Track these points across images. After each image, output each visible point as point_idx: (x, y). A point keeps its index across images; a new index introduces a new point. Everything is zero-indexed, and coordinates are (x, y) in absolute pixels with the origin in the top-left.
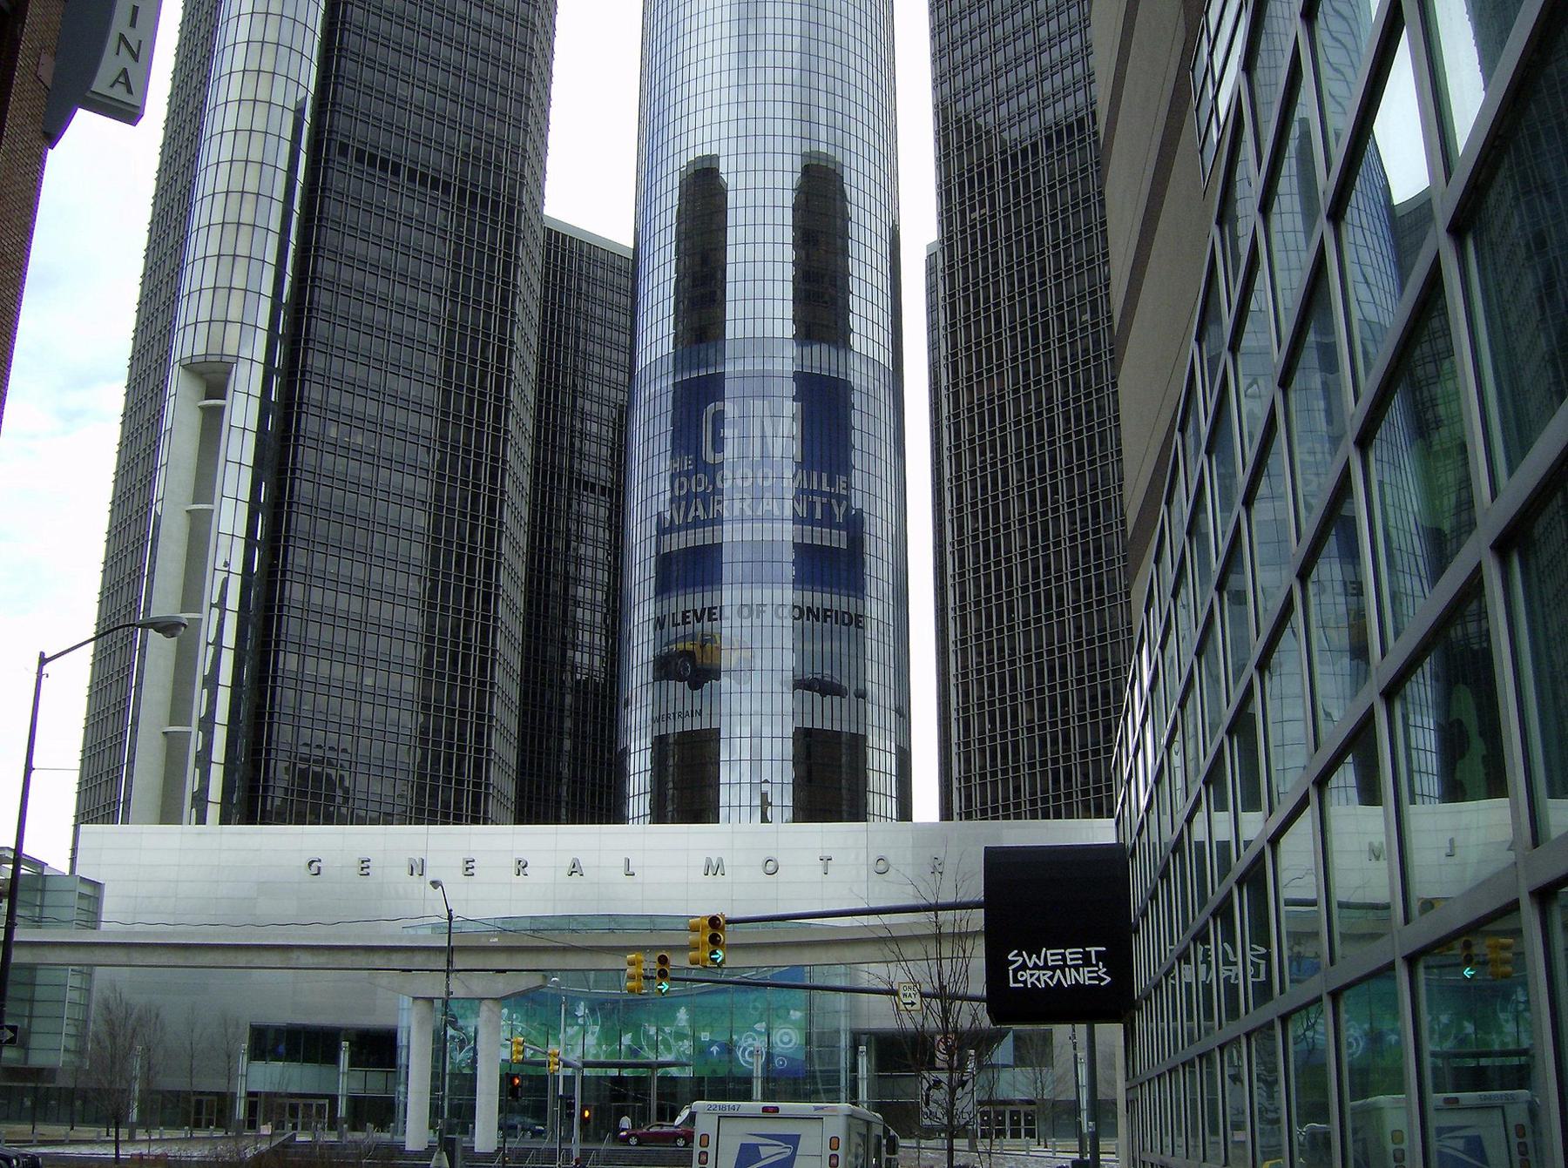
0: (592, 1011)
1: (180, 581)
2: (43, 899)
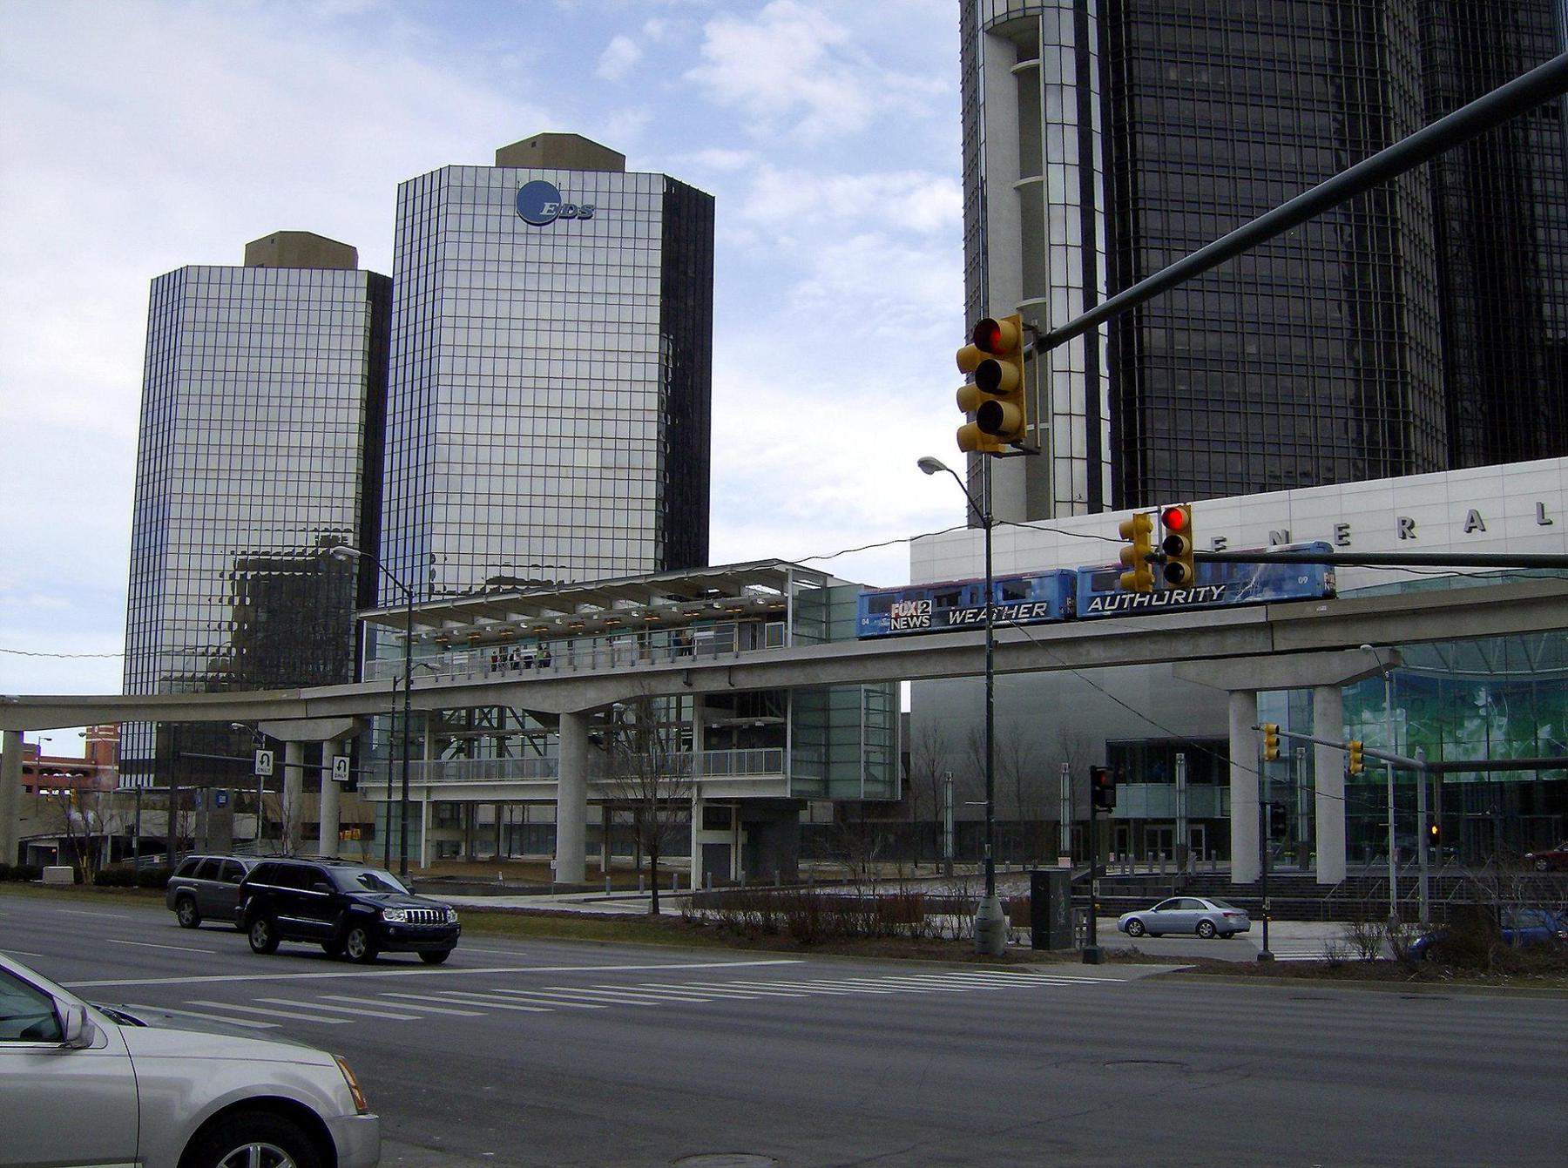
0: (1497, 698)
1: (1018, 266)
2: (828, 615)
